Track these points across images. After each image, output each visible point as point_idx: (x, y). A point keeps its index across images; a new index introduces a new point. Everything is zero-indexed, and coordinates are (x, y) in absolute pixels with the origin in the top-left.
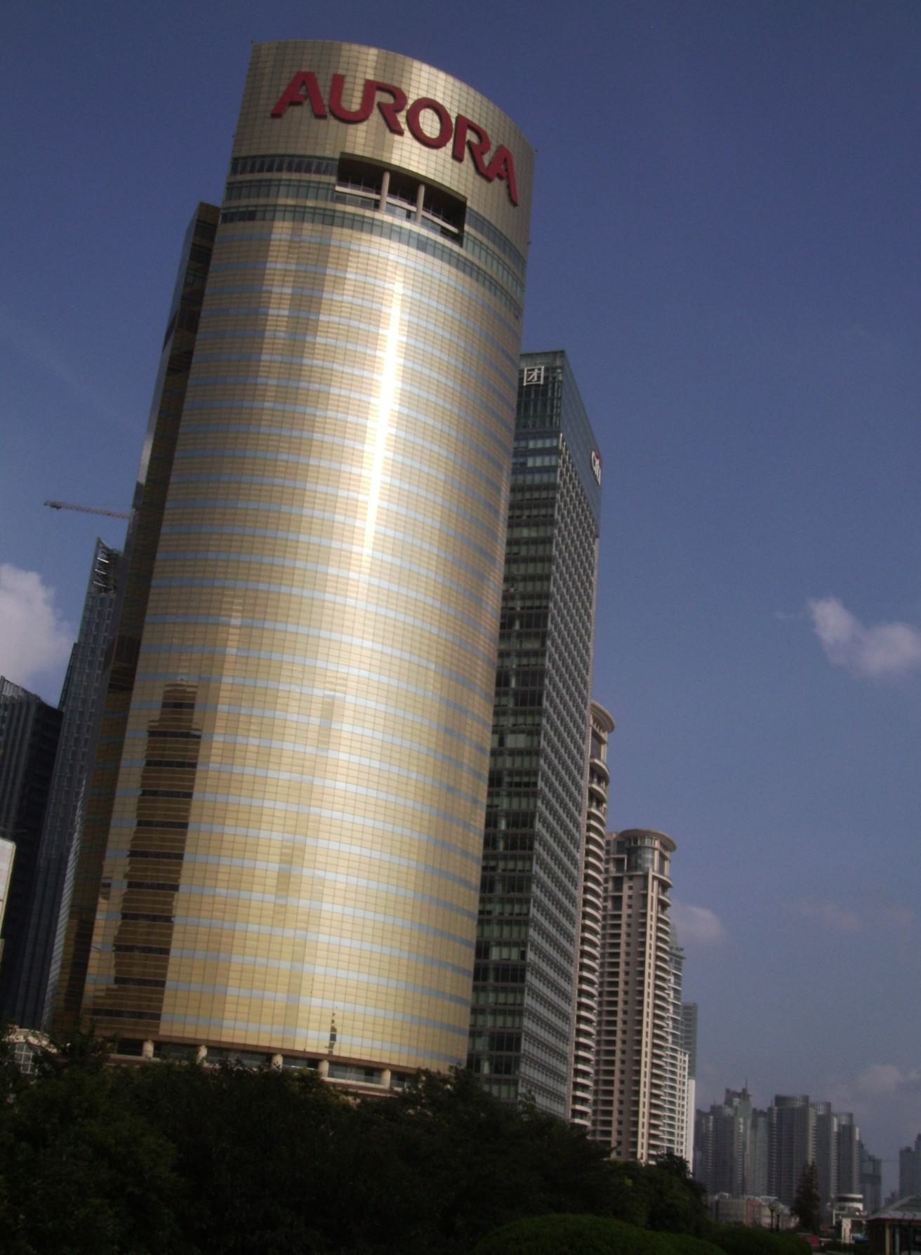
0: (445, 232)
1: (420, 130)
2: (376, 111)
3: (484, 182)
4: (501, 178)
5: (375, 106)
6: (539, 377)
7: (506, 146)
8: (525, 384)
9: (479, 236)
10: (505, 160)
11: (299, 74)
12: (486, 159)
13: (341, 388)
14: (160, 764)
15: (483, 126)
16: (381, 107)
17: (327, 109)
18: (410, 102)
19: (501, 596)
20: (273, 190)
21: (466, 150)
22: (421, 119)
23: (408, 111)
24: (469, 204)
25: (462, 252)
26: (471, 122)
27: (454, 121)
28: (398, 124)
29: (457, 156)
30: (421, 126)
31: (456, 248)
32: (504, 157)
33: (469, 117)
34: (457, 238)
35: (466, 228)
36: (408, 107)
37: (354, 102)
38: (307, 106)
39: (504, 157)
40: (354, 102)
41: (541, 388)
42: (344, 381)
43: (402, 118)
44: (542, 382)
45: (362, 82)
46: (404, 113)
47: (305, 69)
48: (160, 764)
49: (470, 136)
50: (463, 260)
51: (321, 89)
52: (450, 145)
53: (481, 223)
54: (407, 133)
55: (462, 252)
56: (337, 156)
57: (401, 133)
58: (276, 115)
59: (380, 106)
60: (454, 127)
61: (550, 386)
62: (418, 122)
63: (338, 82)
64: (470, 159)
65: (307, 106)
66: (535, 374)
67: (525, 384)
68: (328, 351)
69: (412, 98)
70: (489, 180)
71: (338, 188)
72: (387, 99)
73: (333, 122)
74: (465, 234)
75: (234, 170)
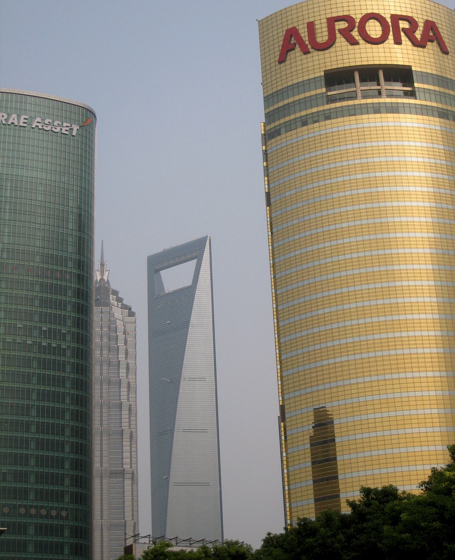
1: (368, 36)
2: (338, 35)
4: (432, 41)
5: (337, 32)
7: (430, 19)
9: (426, 86)
10: (432, 28)
11: (288, 31)
12: (418, 35)
13: (393, 265)
14: (323, 499)
15: (410, 14)
16: (341, 31)
17: (309, 47)
21: (402, 34)
22: (367, 28)
24: (413, 69)
25: (417, 102)
26: (401, 15)
27: (389, 20)
28: (353, 38)
29: (398, 41)
30: (368, 32)
32: (430, 26)
33: (399, 13)
34: (412, 94)
35: (416, 85)
36: (357, 24)
37: (322, 36)
38: (298, 49)
40: (322, 36)
42: (394, 259)
43: (355, 33)
45: (325, 20)
46: (356, 29)
47: (290, 27)
48: (323, 499)
49: (404, 25)
50: (433, 92)
51: (302, 35)
52: (391, 37)
53: (426, 77)
54: (361, 42)
55: (417, 102)
56: (322, 74)
57: (357, 43)
58: (282, 60)
60: (390, 24)
62: (366, 31)
63: (311, 26)
64: (407, 39)
68: (351, 168)
69: (358, 18)
70: (424, 47)
71: (329, 93)
72: (342, 25)
73: (316, 53)
74: (416, 89)
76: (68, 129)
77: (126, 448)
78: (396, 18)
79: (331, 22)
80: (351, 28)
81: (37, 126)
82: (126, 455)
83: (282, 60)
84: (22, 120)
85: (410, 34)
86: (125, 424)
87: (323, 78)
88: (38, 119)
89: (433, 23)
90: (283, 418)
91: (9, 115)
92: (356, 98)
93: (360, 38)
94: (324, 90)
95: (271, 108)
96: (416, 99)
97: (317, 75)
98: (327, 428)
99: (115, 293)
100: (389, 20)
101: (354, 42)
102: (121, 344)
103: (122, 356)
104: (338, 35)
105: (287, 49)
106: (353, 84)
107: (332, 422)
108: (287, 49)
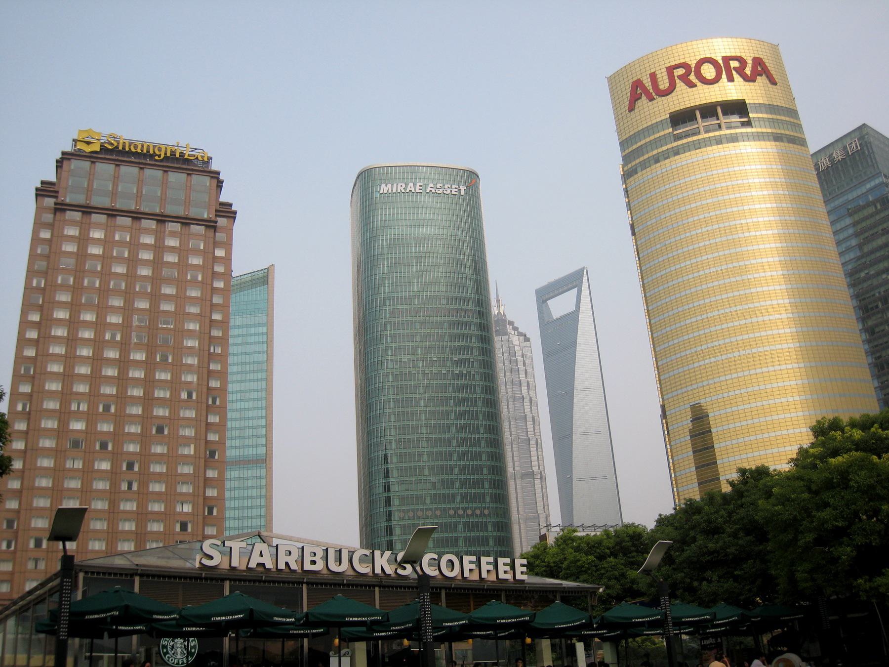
0: (743, 124)
1: (704, 78)
2: (678, 81)
3: (751, 84)
5: (676, 78)
6: (856, 146)
7: (757, 56)
8: (850, 154)
9: (760, 115)
12: (748, 71)
15: (739, 54)
16: (680, 77)
17: (654, 94)
18: (693, 66)
19: (854, 317)
20: (645, 150)
21: (734, 72)
23: (694, 71)
24: (747, 101)
25: (754, 130)
27: (721, 62)
29: (731, 79)
31: (749, 130)
32: (757, 62)
34: (748, 124)
35: (751, 115)
37: (664, 84)
38: (644, 97)
39: (757, 62)
40: (664, 84)
41: (860, 152)
43: (692, 77)
44: (859, 148)
45: (665, 70)
46: (693, 73)
49: (734, 64)
51: (647, 85)
52: (724, 76)
53: (759, 107)
54: (699, 84)
55: (754, 130)
56: (668, 116)
57: (695, 86)
58: (631, 109)
59: (679, 77)
61: (865, 148)
63: (653, 76)
65: (644, 97)
66: (854, 145)
67: (850, 154)
70: (754, 81)
71: (675, 132)
72: (680, 72)
74: (752, 119)
75: (654, 99)
76: (457, 190)
77: (534, 453)
78: (727, 59)
79: (670, 70)
80: (688, 73)
81: (430, 191)
82: (534, 458)
83: (631, 109)
84: (418, 187)
85: (740, 71)
86: (531, 433)
87: (669, 120)
88: (432, 185)
89: (760, 59)
90: (664, 415)
91: (407, 185)
92: (699, 133)
93: (697, 81)
94: (671, 130)
95: (627, 152)
96: (752, 127)
97: (663, 118)
98: (703, 421)
99: (511, 323)
100: (721, 62)
101: (692, 85)
102: (521, 366)
103: (522, 376)
104: (678, 81)
105: (634, 99)
106: (695, 122)
107: (708, 416)
108: (634, 99)
